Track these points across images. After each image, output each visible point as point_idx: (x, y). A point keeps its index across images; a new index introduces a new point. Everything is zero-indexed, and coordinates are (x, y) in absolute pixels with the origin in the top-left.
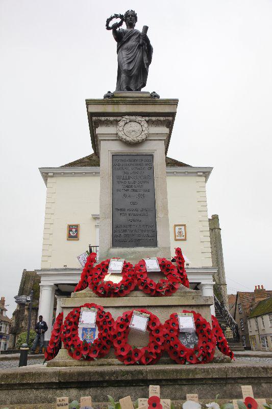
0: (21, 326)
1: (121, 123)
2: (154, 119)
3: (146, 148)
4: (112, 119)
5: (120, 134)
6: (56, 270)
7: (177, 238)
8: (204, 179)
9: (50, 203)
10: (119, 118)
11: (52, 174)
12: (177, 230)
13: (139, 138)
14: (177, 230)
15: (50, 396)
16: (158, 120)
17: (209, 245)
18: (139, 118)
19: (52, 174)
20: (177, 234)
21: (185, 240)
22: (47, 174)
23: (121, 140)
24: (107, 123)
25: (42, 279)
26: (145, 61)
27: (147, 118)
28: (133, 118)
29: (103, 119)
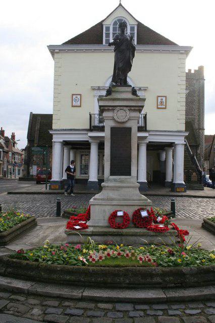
0: (32, 160)
1: (115, 111)
2: (132, 108)
3: (128, 125)
4: (111, 108)
5: (115, 117)
6: (65, 130)
7: (159, 107)
8: (185, 55)
9: (57, 68)
10: (114, 108)
11: (58, 51)
12: (159, 100)
13: (124, 120)
14: (159, 100)
15: (143, 281)
16: (135, 109)
17: (184, 113)
18: (125, 108)
19: (58, 51)
20: (159, 104)
21: (165, 108)
22: (53, 50)
23: (114, 119)
24: (108, 110)
25: (54, 136)
26: (131, 56)
27: (129, 108)
28: (122, 108)
29: (106, 108)
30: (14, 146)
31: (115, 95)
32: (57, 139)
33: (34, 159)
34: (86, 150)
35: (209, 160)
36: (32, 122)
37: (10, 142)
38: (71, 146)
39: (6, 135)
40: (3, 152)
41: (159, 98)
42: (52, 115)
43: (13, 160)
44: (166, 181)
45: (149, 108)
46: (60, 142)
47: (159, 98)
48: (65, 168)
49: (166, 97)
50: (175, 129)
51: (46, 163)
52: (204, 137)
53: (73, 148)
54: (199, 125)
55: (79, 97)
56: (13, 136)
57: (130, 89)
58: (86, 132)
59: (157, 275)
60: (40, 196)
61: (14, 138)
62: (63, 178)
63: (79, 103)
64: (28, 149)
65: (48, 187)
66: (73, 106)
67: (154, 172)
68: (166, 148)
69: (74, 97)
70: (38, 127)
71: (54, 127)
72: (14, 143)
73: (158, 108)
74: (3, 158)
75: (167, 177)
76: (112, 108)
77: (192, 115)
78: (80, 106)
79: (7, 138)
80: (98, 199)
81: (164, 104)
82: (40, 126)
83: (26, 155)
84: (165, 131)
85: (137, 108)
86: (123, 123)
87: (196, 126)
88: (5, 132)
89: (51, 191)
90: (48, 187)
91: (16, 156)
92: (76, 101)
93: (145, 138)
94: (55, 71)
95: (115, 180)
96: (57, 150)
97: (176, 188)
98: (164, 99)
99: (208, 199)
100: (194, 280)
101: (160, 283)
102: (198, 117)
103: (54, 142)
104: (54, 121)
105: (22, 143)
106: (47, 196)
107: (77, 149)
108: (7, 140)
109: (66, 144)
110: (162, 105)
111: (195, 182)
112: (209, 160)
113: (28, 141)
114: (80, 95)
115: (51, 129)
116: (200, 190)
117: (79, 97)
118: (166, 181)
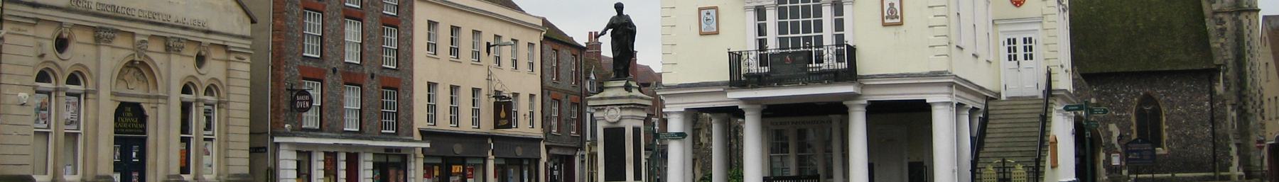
3: (622, 124)
50: (926, 70)
63: (714, 25)
66: (702, 34)
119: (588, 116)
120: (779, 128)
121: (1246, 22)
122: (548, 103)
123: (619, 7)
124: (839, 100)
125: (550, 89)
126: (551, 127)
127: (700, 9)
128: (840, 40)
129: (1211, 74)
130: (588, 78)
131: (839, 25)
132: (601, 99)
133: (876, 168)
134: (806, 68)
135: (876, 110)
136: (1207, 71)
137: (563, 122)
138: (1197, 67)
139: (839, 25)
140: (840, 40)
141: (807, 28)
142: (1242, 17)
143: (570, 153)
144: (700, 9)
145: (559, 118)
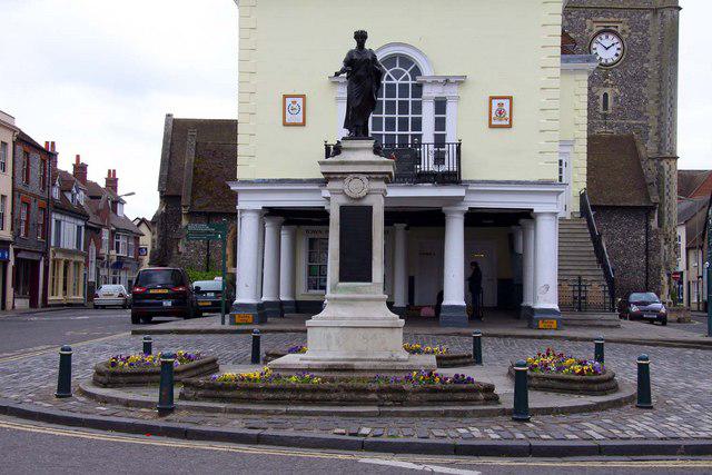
1: (347, 181)
3: (366, 202)
7: (493, 123)
17: (586, 127)
18: (361, 176)
20: (494, 115)
21: (510, 126)
24: (335, 179)
25: (241, 198)
29: (332, 176)
30: (115, 211)
31: (344, 156)
32: (249, 204)
33: (182, 248)
34: (321, 228)
35: (701, 247)
36: (172, 144)
37: (107, 198)
38: (281, 219)
39: (91, 177)
40: (87, 227)
41: (495, 102)
42: (229, 128)
43: (113, 252)
44: (524, 304)
45: (466, 124)
46: (254, 211)
47: (495, 102)
48: (281, 373)
49: (511, 98)
51: (221, 258)
52: (675, 177)
53: (287, 223)
54: (661, 145)
55: (300, 101)
56: (112, 181)
57: (371, 144)
58: (317, 187)
59: (373, 391)
60: (212, 337)
61: (115, 188)
62: (264, 299)
64: (165, 222)
65: (227, 321)
66: (285, 124)
67: (500, 281)
68: (522, 221)
69: (289, 101)
70: (189, 158)
71: (240, 176)
72: (117, 202)
73: (491, 126)
74: (86, 248)
75: (525, 296)
76: (342, 176)
77: (639, 115)
78: (304, 124)
79: (95, 185)
80: (325, 319)
81: (508, 116)
82: (200, 158)
83: (156, 237)
84: (509, 182)
85: (380, 176)
86: (359, 199)
87: (648, 148)
88: (88, 169)
89: (236, 327)
90: (227, 321)
91: (122, 241)
92: (294, 111)
93: (461, 199)
94: (241, 38)
95: (347, 288)
96: (248, 229)
97: (538, 320)
98: (507, 102)
99: (623, 345)
100: (416, 397)
101: (376, 401)
102: (656, 123)
103: (242, 211)
104: (240, 161)
105: (142, 201)
106: (226, 336)
107: (299, 223)
108: (94, 193)
109: (270, 212)
110: (501, 115)
111: (601, 308)
112: (701, 247)
113: (161, 197)
114: (303, 96)
115: (234, 178)
116: (611, 327)
117: (300, 101)
118: (524, 304)
119: (53, 220)
120: (312, 236)
121: (666, 167)
122: (18, 205)
123: (361, 37)
124: (435, 205)
125: (20, 191)
126: (19, 230)
127: (285, 97)
128: (440, 141)
129: (648, 211)
130: (54, 185)
131: (440, 124)
132: (343, 163)
133: (416, 283)
134: (413, 169)
135: (475, 219)
136: (646, 207)
137: (31, 226)
138: (636, 203)
139: (440, 124)
140: (440, 141)
141: (403, 124)
142: (664, 163)
143: (36, 257)
144: (285, 97)
145: (27, 222)
